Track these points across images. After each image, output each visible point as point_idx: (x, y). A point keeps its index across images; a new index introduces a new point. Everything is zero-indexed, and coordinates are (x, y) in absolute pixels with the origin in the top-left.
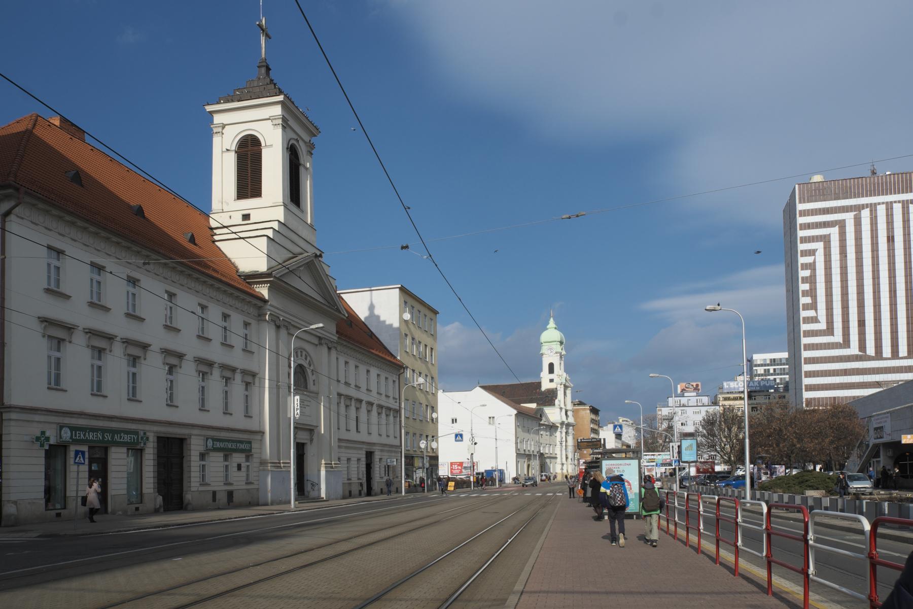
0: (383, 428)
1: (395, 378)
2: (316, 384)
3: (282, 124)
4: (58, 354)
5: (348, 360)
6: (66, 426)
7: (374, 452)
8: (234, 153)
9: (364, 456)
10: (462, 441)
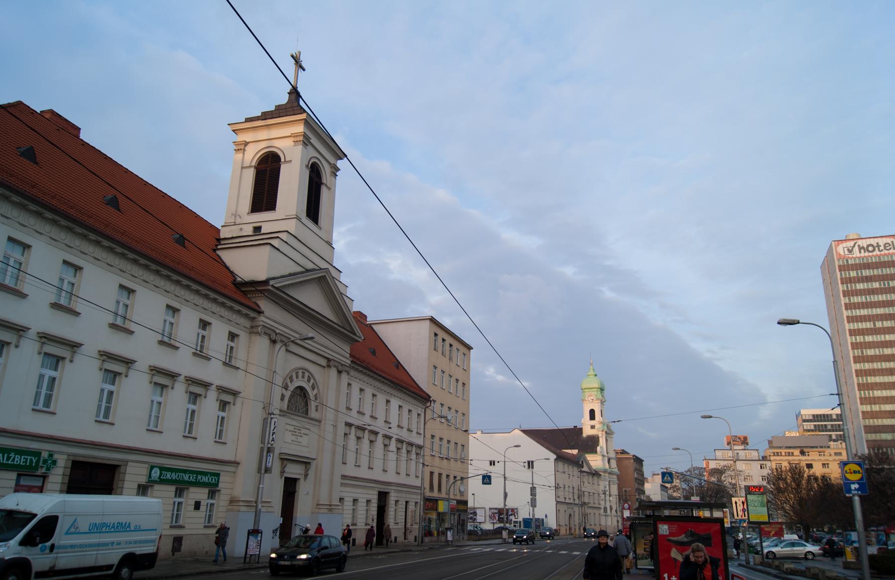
0: (403, 464)
1: (421, 411)
2: (319, 410)
3: (303, 141)
4: (112, 388)
5: (363, 387)
6: (157, 466)
7: (389, 493)
8: (253, 169)
9: (376, 497)
10: (490, 484)
